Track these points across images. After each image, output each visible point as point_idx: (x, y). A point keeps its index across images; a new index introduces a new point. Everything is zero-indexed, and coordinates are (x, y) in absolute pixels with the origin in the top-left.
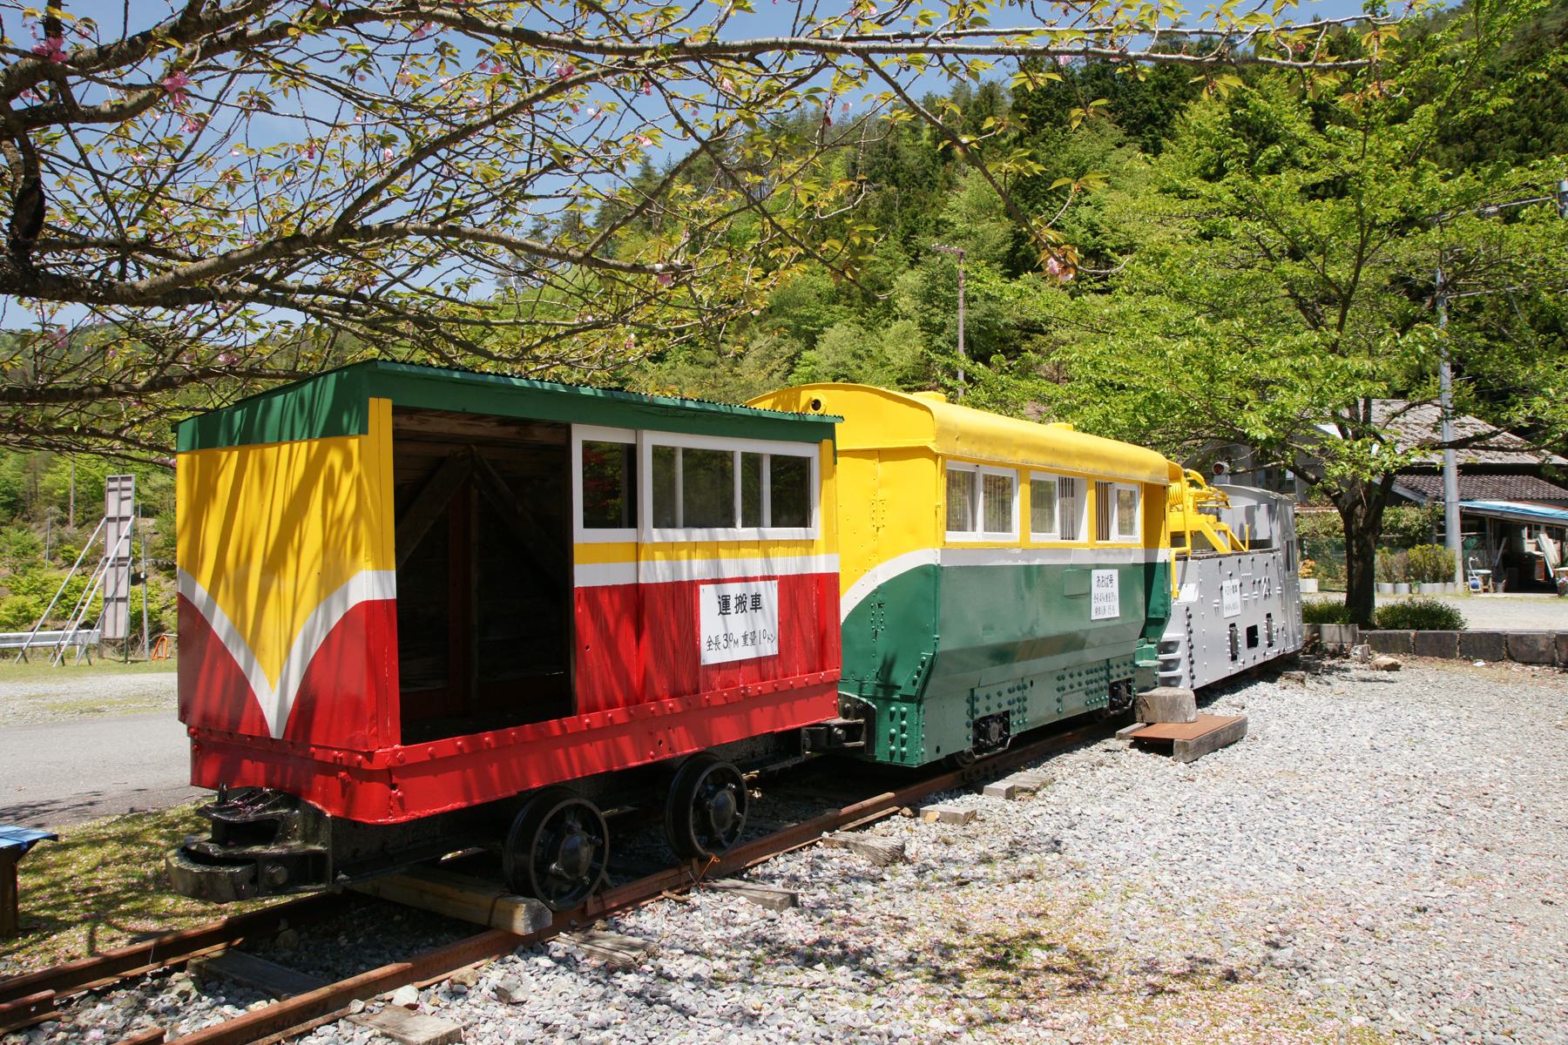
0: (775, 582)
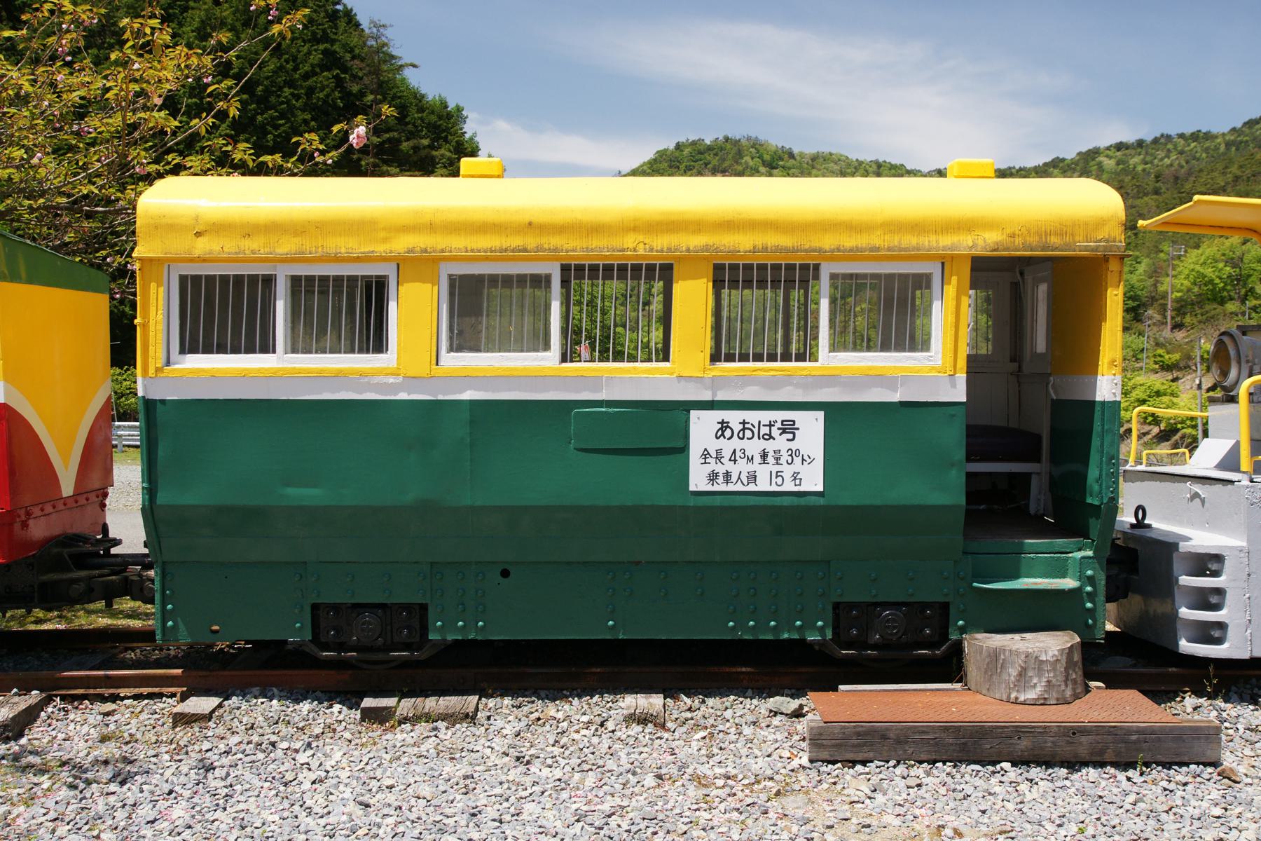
0: (820, 414)
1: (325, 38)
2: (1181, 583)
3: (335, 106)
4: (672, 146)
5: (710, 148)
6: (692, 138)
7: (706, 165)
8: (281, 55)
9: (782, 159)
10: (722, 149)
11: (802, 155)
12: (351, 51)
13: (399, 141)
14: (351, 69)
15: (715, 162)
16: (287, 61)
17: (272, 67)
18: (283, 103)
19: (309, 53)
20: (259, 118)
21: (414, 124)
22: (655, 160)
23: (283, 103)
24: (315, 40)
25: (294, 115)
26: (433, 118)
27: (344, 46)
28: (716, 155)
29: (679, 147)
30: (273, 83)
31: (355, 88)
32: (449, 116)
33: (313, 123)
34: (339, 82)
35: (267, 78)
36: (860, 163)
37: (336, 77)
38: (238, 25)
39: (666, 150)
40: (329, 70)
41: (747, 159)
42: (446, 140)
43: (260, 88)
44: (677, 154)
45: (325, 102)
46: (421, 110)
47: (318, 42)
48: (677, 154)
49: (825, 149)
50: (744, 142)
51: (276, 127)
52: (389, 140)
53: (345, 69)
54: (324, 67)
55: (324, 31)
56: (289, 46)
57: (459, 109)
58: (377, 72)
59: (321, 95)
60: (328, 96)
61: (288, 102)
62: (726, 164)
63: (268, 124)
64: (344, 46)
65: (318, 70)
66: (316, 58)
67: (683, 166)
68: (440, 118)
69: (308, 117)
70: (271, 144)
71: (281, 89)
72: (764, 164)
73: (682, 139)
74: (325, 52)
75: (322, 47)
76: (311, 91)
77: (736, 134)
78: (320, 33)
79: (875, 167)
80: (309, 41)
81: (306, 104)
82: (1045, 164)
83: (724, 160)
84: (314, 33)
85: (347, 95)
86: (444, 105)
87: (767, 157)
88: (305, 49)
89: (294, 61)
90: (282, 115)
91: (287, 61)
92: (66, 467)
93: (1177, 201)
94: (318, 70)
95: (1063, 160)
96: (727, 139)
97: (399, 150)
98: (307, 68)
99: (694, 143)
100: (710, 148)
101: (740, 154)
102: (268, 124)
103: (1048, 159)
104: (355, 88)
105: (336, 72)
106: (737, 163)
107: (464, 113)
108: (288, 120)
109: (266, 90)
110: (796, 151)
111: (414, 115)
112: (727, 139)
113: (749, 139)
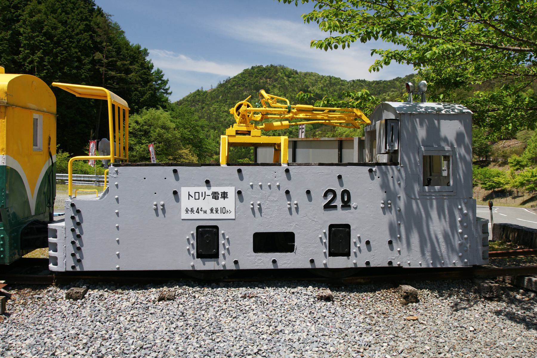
0: (259, 162)
1: (86, 19)
2: (49, 241)
3: (89, 47)
4: (250, 68)
5: (265, 69)
6: (258, 65)
7: (263, 75)
8: (67, 25)
9: (293, 74)
10: (269, 69)
11: (301, 73)
12: (98, 25)
13: (116, 61)
14: (97, 32)
15: (267, 74)
16: (69, 28)
17: (61, 30)
18: (65, 45)
19: (79, 25)
20: (55, 50)
21: (124, 56)
22: (243, 73)
23: (65, 45)
24: (82, 20)
25: (70, 50)
26: (132, 53)
27: (95, 23)
28: (267, 72)
29: (253, 68)
30: (61, 36)
31: (98, 40)
32: (140, 52)
33: (79, 53)
34: (91, 37)
35: (59, 34)
36: (323, 77)
37: (91, 35)
38: (48, 13)
39: (248, 69)
40: (88, 32)
41: (279, 74)
42: (137, 62)
43: (56, 38)
44: (252, 71)
45: (85, 45)
46: (127, 50)
47: (84, 21)
48: (252, 71)
49: (310, 71)
50: (278, 67)
51: (62, 54)
52: (112, 61)
53: (95, 32)
54: (85, 31)
55: (86, 16)
56: (71, 22)
57: (146, 50)
58: (106, 33)
59: (83, 42)
60: (86, 42)
61: (68, 45)
62: (271, 76)
63: (59, 53)
64: (95, 23)
65: (82, 32)
66: (82, 27)
67: (254, 76)
68: (135, 53)
69: (77, 50)
70: (59, 61)
71: (65, 39)
72: (286, 76)
73: (254, 65)
74: (86, 25)
75: (85, 23)
76: (78, 42)
77: (275, 64)
78: (84, 17)
79: (329, 78)
80: (80, 20)
81: (77, 45)
82: (394, 80)
83: (270, 74)
84: (82, 17)
85: (94, 42)
86: (138, 48)
87: (287, 73)
88: (78, 24)
89: (72, 28)
90: (65, 50)
91: (69, 28)
92: (33, 196)
93: (84, 73)
94: (82, 32)
95: (401, 78)
96: (272, 66)
97: (117, 65)
98: (78, 31)
99: (259, 67)
100: (265, 69)
101: (276, 72)
102: (59, 53)
103: (395, 78)
104: (98, 40)
105: (90, 33)
106: (275, 75)
107: (148, 51)
108: (67, 52)
109: (58, 39)
110: (298, 71)
111: (124, 51)
112: (272, 66)
113: (280, 66)
